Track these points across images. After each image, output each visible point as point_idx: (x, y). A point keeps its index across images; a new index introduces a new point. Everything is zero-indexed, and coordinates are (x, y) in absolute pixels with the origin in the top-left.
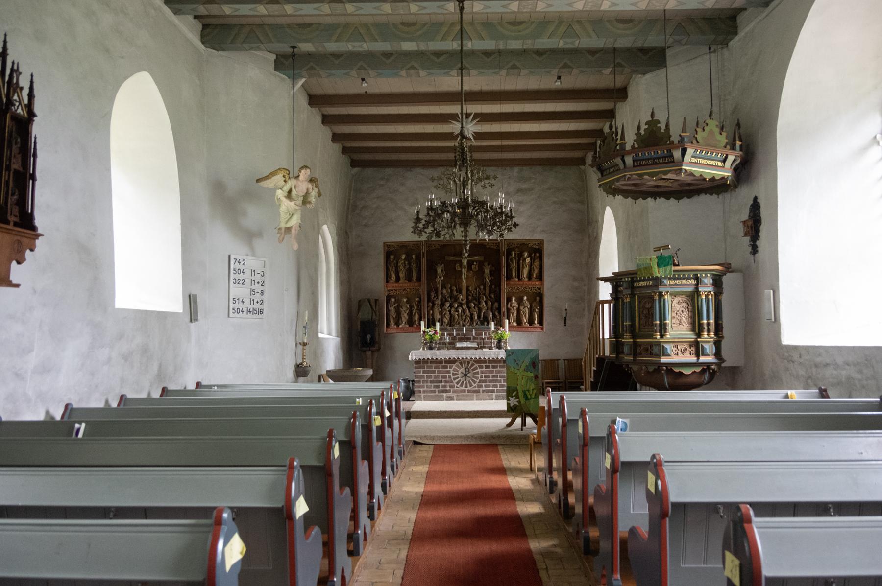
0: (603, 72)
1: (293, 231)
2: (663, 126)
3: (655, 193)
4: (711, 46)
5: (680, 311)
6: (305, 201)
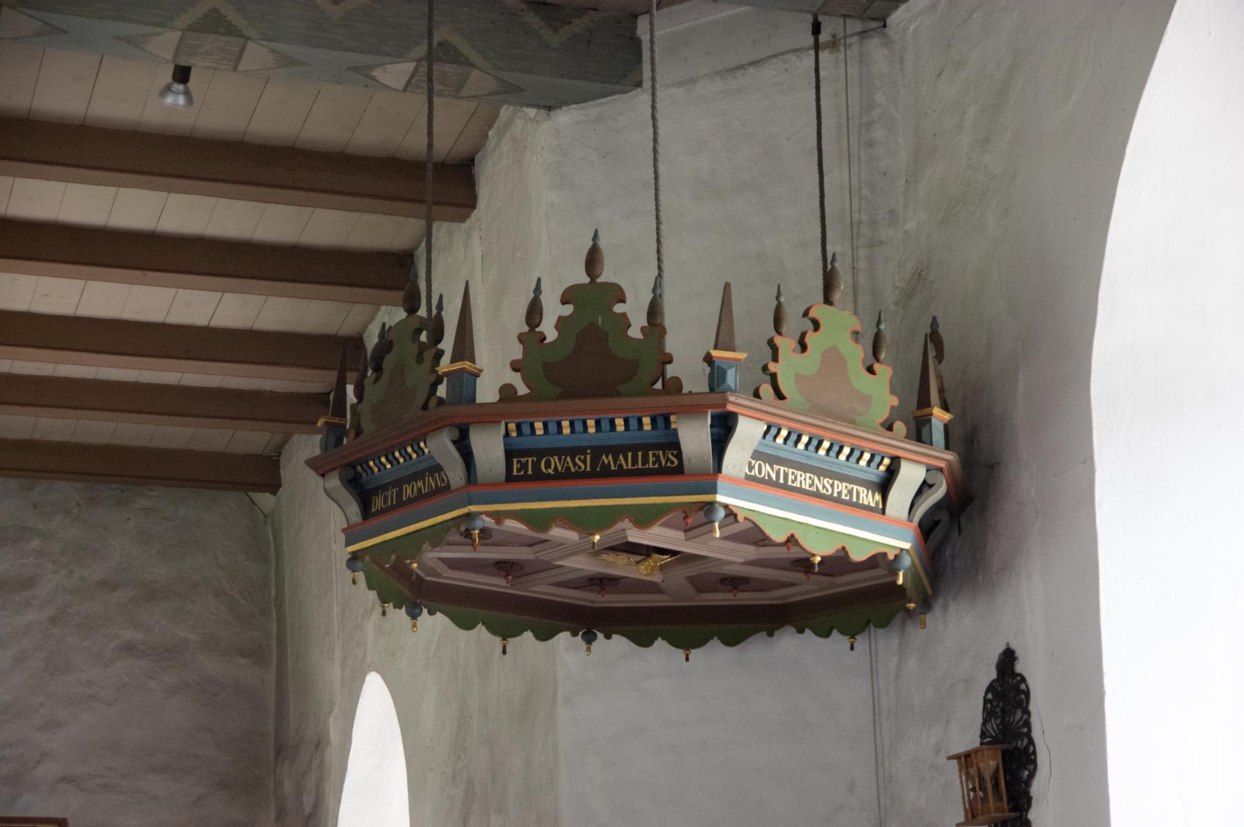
0: (377, 73)
2: (635, 310)
4: (821, 18)
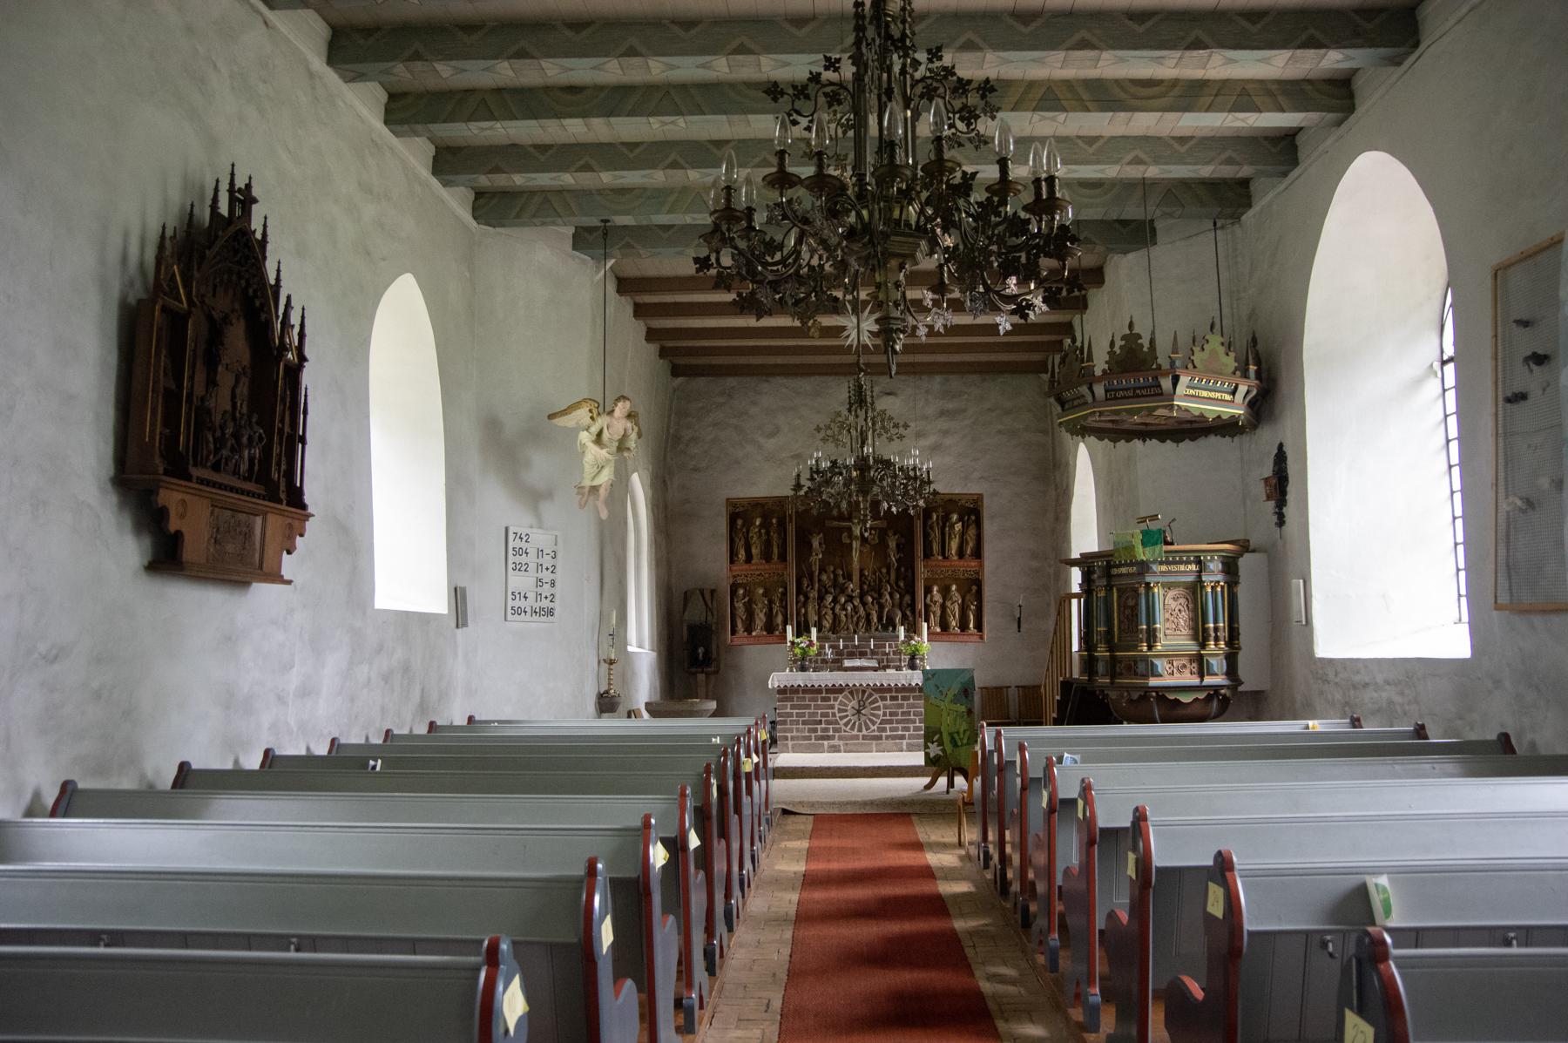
1: (602, 491)
2: (1145, 342)
3: (1144, 434)
4: (1217, 220)
5: (1177, 611)
6: (622, 447)
